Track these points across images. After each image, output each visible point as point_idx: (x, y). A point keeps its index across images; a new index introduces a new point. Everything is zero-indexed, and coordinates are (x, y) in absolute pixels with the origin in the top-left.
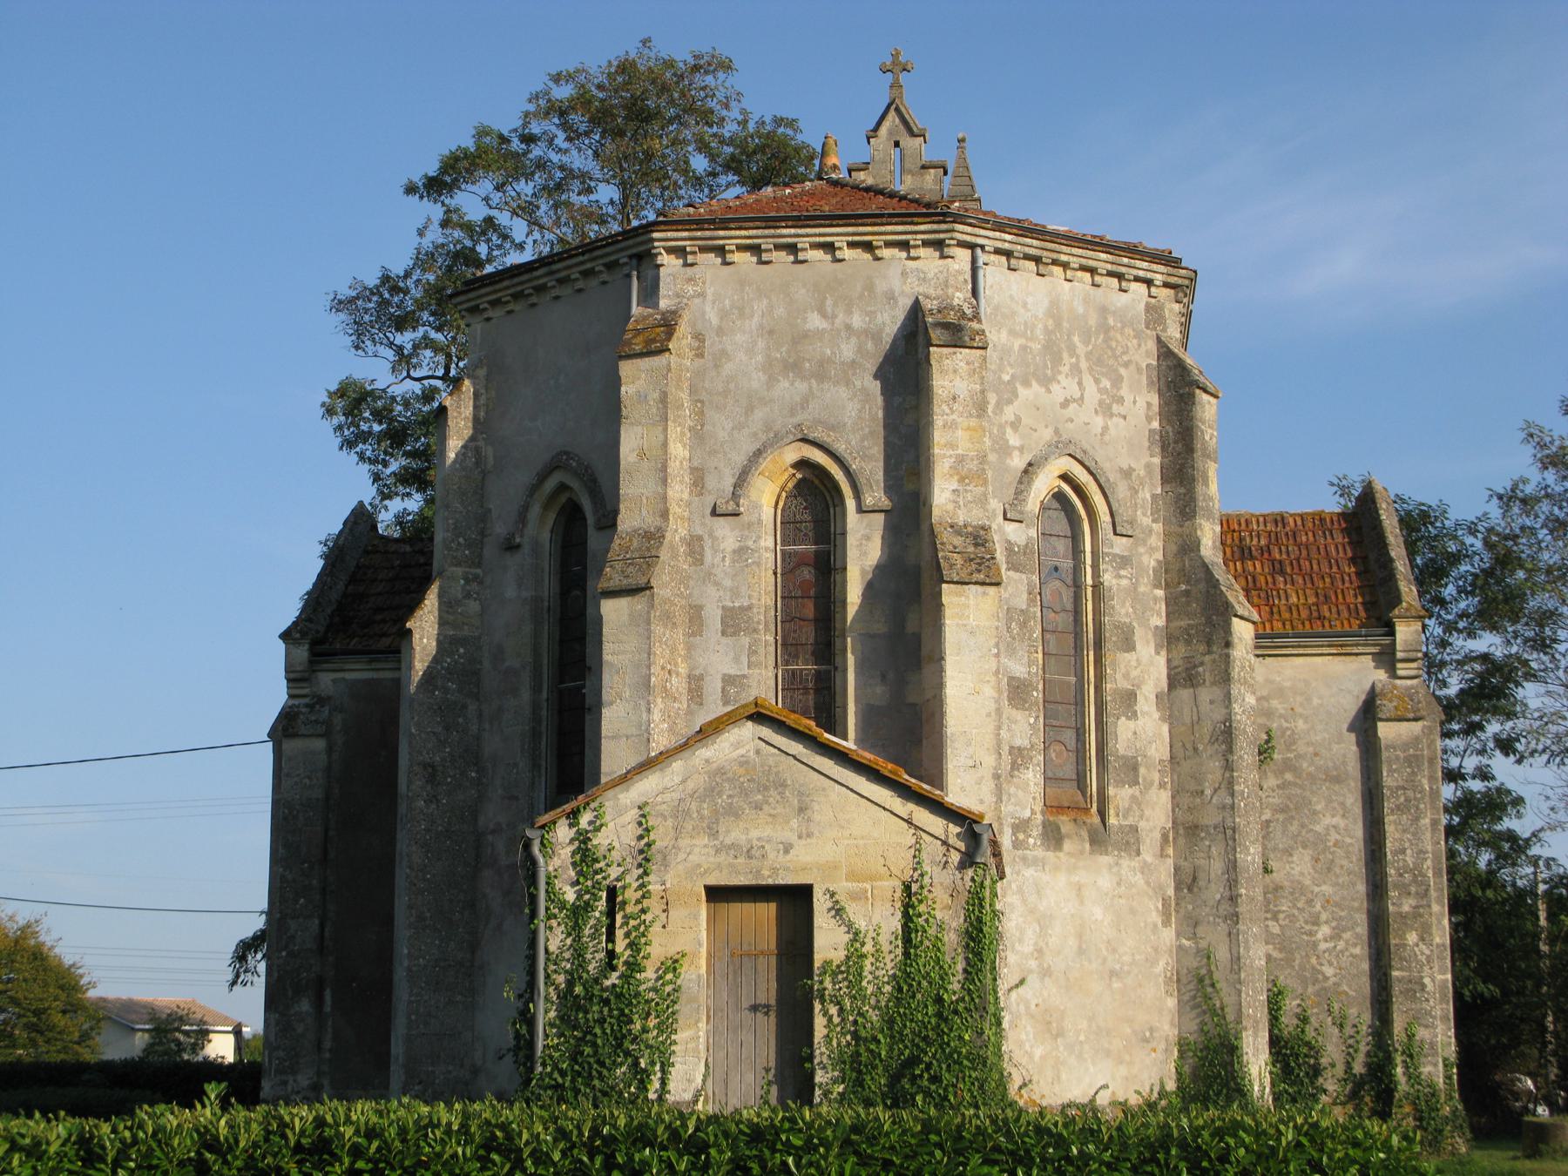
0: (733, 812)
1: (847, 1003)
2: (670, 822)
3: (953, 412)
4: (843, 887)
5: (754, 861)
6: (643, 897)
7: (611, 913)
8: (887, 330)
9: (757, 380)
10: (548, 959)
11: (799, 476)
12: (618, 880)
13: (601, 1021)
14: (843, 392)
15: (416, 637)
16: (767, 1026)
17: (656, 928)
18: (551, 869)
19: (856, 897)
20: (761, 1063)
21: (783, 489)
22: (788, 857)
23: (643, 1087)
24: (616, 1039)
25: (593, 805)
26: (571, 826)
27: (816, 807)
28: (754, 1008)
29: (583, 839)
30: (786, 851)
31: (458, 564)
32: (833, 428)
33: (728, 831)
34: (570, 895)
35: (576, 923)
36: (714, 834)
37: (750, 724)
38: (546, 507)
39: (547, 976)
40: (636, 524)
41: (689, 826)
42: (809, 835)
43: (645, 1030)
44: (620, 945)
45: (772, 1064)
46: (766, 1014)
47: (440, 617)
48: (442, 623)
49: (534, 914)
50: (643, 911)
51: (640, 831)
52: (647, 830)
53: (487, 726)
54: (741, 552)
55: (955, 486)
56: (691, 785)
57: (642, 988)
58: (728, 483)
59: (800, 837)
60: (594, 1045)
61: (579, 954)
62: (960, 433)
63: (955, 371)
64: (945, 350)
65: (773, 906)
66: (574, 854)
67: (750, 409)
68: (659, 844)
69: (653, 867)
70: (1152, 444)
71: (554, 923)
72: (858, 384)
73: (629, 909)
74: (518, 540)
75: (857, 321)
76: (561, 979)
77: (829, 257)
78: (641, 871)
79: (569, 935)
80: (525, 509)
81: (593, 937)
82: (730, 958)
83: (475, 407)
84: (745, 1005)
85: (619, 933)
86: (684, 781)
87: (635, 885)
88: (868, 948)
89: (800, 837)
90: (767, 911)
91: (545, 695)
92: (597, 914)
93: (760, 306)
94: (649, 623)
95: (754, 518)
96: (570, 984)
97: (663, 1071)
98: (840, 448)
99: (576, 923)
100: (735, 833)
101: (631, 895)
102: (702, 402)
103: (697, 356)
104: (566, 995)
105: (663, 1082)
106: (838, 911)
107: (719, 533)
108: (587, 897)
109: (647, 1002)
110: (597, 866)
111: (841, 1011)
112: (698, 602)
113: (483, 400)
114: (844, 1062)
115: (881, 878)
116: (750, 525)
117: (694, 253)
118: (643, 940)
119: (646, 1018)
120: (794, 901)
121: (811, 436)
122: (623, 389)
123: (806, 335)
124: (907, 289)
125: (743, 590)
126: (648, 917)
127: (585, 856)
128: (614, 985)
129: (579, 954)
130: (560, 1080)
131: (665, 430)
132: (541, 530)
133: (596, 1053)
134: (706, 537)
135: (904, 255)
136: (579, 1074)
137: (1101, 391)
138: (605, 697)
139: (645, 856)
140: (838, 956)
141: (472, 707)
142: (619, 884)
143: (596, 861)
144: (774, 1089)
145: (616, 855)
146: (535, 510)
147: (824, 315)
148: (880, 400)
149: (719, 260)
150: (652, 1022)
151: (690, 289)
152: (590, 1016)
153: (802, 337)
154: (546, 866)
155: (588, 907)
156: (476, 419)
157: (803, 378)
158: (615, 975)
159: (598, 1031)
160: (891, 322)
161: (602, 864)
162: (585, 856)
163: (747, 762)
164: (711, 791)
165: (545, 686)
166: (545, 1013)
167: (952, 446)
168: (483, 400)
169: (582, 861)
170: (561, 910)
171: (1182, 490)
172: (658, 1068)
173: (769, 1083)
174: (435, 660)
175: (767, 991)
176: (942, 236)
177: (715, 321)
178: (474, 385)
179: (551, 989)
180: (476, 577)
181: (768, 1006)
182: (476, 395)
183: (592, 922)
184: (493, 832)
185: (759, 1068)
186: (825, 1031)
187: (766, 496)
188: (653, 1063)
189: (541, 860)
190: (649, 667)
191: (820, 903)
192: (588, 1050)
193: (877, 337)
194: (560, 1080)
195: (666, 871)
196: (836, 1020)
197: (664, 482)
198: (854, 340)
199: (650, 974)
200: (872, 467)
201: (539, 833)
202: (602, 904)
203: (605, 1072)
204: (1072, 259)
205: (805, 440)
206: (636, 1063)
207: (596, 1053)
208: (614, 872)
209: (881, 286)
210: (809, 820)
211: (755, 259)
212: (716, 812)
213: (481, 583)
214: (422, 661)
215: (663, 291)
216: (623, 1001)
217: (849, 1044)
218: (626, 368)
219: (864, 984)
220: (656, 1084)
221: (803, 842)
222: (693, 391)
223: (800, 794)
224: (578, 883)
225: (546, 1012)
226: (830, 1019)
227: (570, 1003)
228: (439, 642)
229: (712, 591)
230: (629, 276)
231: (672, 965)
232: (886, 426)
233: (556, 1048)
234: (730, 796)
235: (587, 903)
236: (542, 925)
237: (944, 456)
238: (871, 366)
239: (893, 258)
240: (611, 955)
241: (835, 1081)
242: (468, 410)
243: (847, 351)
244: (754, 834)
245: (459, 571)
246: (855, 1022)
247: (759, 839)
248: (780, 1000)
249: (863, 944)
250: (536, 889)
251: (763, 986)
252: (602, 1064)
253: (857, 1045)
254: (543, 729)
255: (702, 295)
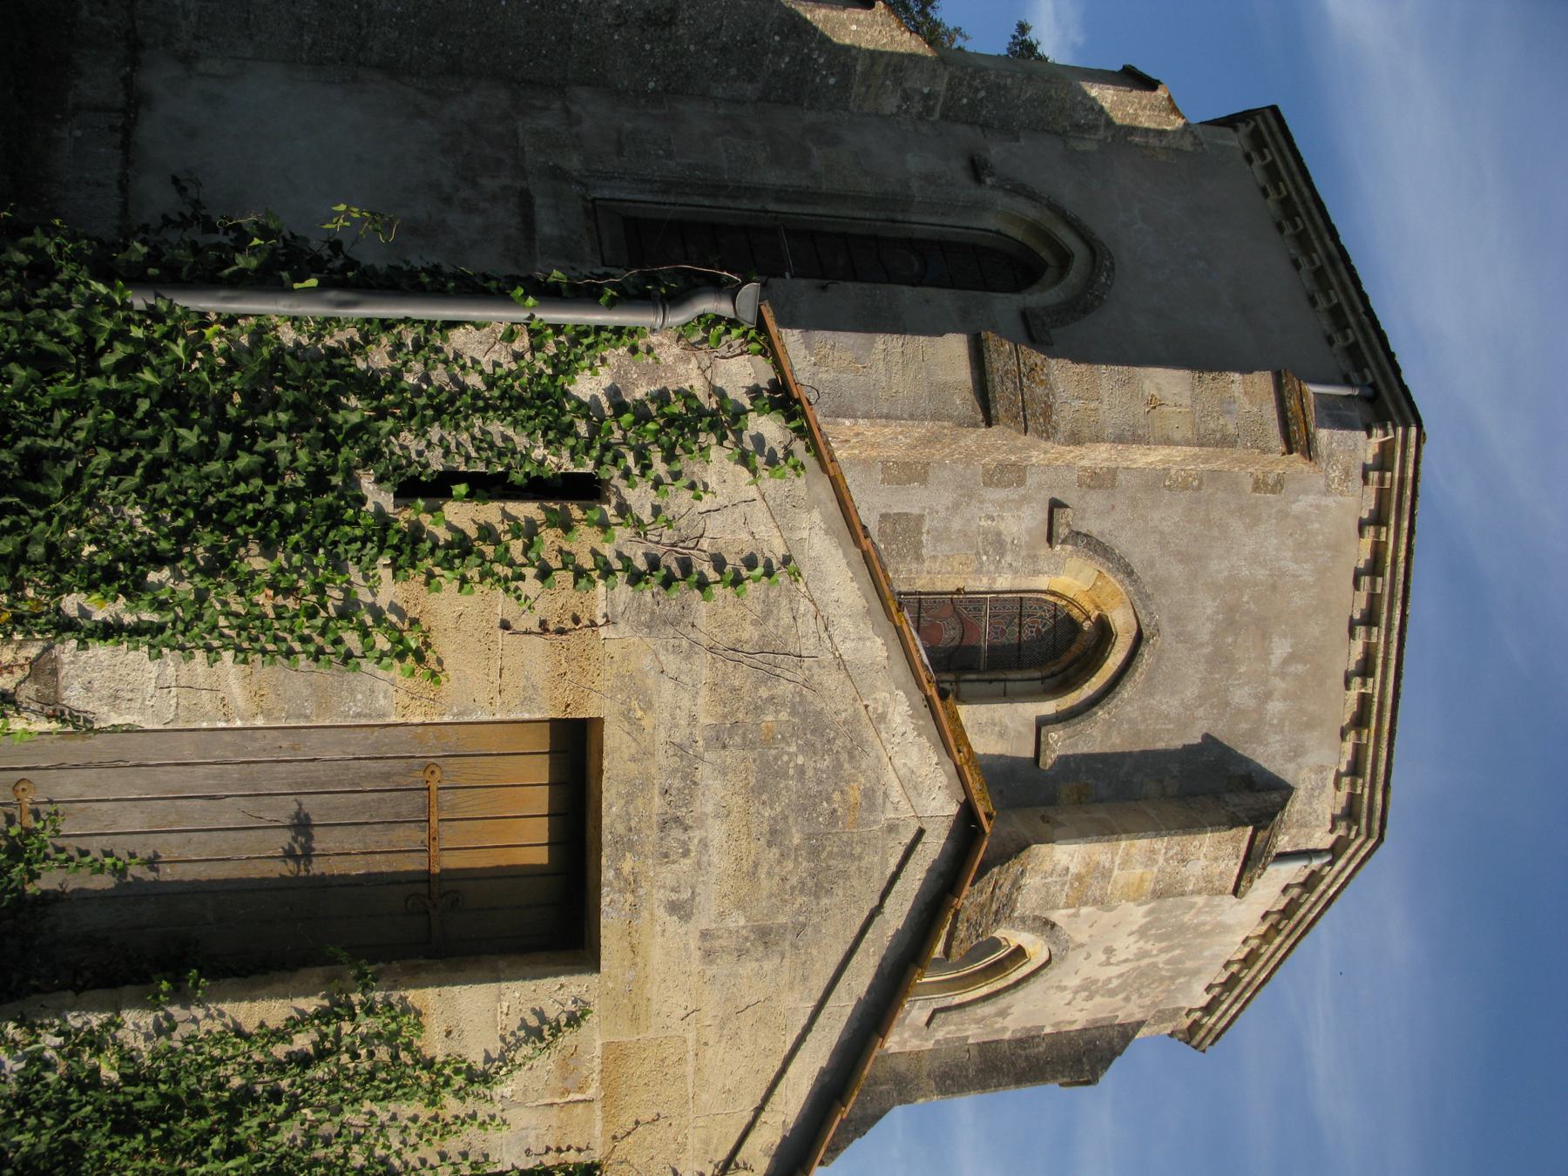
0: (763, 785)
1: (320, 1072)
2: (749, 633)
3: (1167, 860)
4: (593, 1038)
5: (653, 835)
6: (580, 573)
7: (539, 488)
8: (1260, 749)
9: (1218, 568)
10: (429, 325)
11: (1087, 625)
12: (623, 509)
13: (269, 470)
14: (1191, 692)
15: (862, 14)
16: (259, 856)
17: (503, 606)
18: (654, 339)
19: (568, 1065)
20: (170, 847)
21: (1071, 602)
22: (661, 913)
23: (100, 579)
24: (223, 508)
25: (799, 446)
26: (754, 392)
27: (768, 966)
28: (302, 825)
29: (723, 419)
30: (674, 908)
31: (950, 87)
32: (1149, 679)
33: (724, 772)
34: (587, 386)
35: (520, 402)
36: (718, 740)
37: (953, 809)
38: (1035, 229)
39: (386, 325)
40: (1060, 388)
41: (740, 678)
42: (708, 955)
43: (245, 584)
44: (462, 514)
45: (168, 873)
46: (289, 854)
47: (882, 54)
48: (874, 56)
49: (550, 294)
50: (545, 574)
51: (733, 560)
52: (737, 581)
53: (721, 111)
54: (998, 544)
55: (1073, 870)
56: (832, 680)
57: (354, 573)
58: (1092, 525)
59: (705, 935)
60: (207, 452)
61: (446, 407)
62: (1139, 870)
63: (1216, 859)
64: (1244, 846)
65: (540, 857)
66: (688, 396)
67: (1183, 557)
68: (700, 607)
69: (649, 592)
70: (1029, 1030)
71: (522, 343)
72: (1200, 712)
73: (549, 538)
74: (989, 181)
75: (1275, 707)
76: (379, 358)
77: (1352, 667)
78: (641, 564)
79: (491, 383)
80: (1032, 196)
81: (483, 442)
82: (416, 773)
83: (1147, 130)
84: (309, 803)
85: (491, 512)
86: (841, 664)
87: (608, 551)
88: (451, 1106)
89: (705, 935)
90: (528, 842)
91: (772, 206)
92: (538, 453)
93: (1306, 572)
94: (936, 417)
95: (1042, 565)
96: (368, 385)
97: (137, 631)
98: (1127, 691)
99: (520, 402)
100: (715, 790)
101: (585, 542)
102: (1199, 488)
103: (1256, 482)
104: (334, 372)
105: (109, 631)
106: (540, 1031)
107: (1026, 512)
108: (582, 428)
109: (319, 589)
110: (656, 456)
111: (303, 1061)
112: (931, 478)
113: (1153, 141)
114: (174, 1078)
115: (607, 1119)
116: (1034, 558)
117: (1382, 481)
118: (473, 573)
119: (273, 585)
120: (551, 917)
121: (1145, 650)
122: (1237, 376)
123: (1265, 636)
124: (1304, 773)
125: (945, 548)
126: (531, 586)
127: (685, 423)
128: (362, 500)
129: (446, 407)
130: (107, 361)
131: (1188, 443)
132: (1000, 216)
133: (187, 458)
134: (1022, 491)
135: (1343, 768)
136: (126, 410)
137: (1109, 980)
138: (818, 335)
139: (672, 573)
140: (434, 1045)
141: (750, 90)
142: (610, 510)
143: (669, 458)
144: (106, 882)
145: (679, 501)
146: (1031, 212)
147: (1286, 662)
148: (1177, 744)
149: (1365, 515)
150: (265, 600)
151: (1335, 474)
152: (282, 440)
153: (1263, 628)
154: (660, 329)
155: (559, 432)
156: (1132, 130)
157: (1214, 634)
158: (387, 501)
159: (244, 461)
160: (1268, 755)
161: (659, 467)
162: (685, 423)
163: (872, 807)
164: (813, 727)
165: (785, 208)
166: (290, 317)
167: (1124, 865)
168: (1153, 141)
169: (671, 421)
170: (554, 362)
171: (971, 1073)
172: (148, 616)
173: (119, 872)
174: (825, 41)
175: (344, 853)
176: (1363, 822)
177: (1296, 508)
178: (1175, 132)
179: (353, 333)
180: (929, 110)
181: (308, 855)
182: (1161, 133)
183: (521, 441)
184: (567, 111)
185: (156, 842)
186: (250, 1026)
187: (1071, 580)
188: (161, 606)
189: (677, 318)
190: (867, 416)
191: (553, 992)
192: (191, 438)
193: (1254, 735)
194: (107, 361)
195: (637, 626)
196: (280, 1050)
197: (1119, 439)
198: (1252, 703)
199: (388, 590)
200: (1097, 737)
201: (748, 316)
202: (559, 462)
203: (131, 482)
204: (1272, 948)
205: (1139, 639)
206: (159, 560)
207: (187, 458)
208: (640, 498)
209: (1311, 738)
210: (741, 953)
211: (1361, 565)
212: (769, 741)
213: (920, 117)
214: (826, 19)
215: (1339, 434)
216: (316, 520)
217: (220, 1086)
218: (1262, 381)
219: (367, 1105)
220: (103, 611)
221: (694, 943)
222: (1215, 475)
223: (799, 930)
224: (620, 408)
225: (294, 319)
226: (281, 1035)
227: (326, 376)
228: (847, 49)
229: (947, 499)
230: (1347, 381)
231: (412, 650)
232: (1144, 753)
233: (197, 344)
234: (801, 771)
235: (568, 430)
236: (522, 315)
237: (1114, 854)
238: (1221, 732)
239: (1341, 753)
240: (438, 488)
241: (127, 1057)
242: (1146, 121)
243: (1241, 696)
244: (716, 832)
245: (941, 87)
246: (275, 1095)
247: (704, 844)
248: (325, 883)
249: (460, 1094)
250: (612, 304)
251: (352, 840)
252: (154, 472)
253: (220, 1106)
254: (722, 202)
255: (1328, 491)
